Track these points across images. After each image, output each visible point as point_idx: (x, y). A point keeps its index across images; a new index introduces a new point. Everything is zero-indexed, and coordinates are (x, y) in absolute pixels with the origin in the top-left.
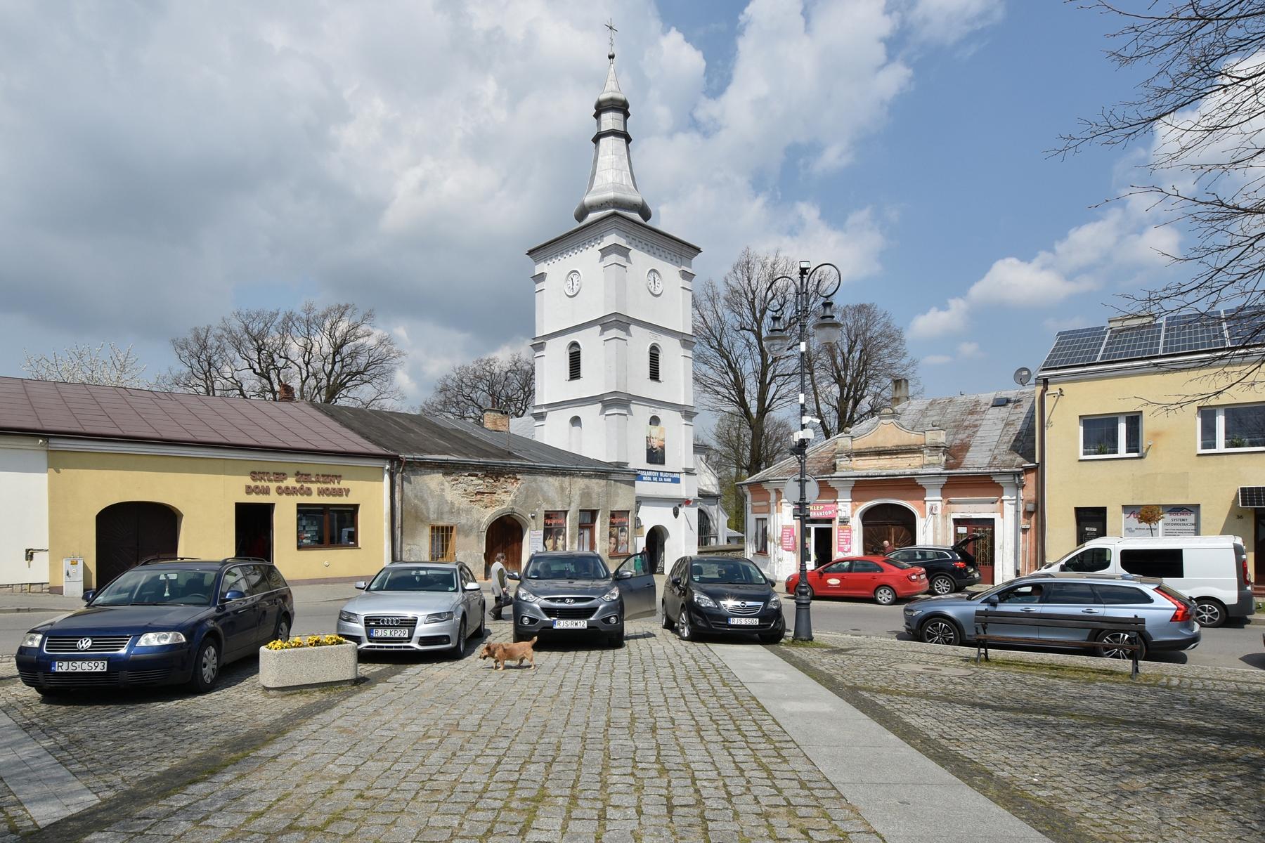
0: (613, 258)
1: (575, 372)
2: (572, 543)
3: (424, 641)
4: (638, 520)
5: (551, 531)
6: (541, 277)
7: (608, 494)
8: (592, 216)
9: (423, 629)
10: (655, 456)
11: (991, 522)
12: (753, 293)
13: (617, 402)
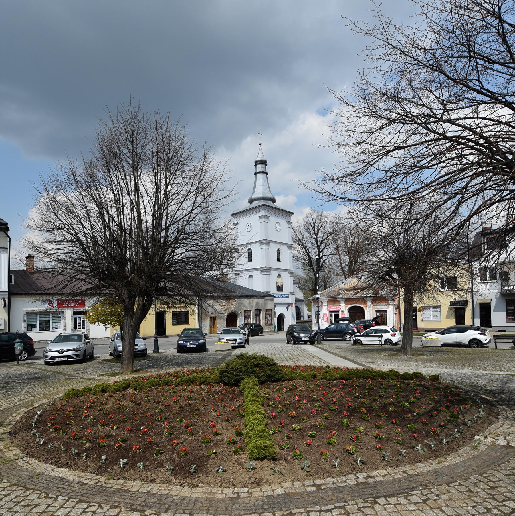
0: (263, 220)
1: (250, 259)
2: (253, 321)
3: (238, 343)
4: (274, 312)
5: (246, 317)
6: (237, 224)
7: (264, 304)
8: (255, 204)
9: (238, 341)
10: (280, 288)
11: (386, 311)
12: (314, 224)
13: (266, 270)
